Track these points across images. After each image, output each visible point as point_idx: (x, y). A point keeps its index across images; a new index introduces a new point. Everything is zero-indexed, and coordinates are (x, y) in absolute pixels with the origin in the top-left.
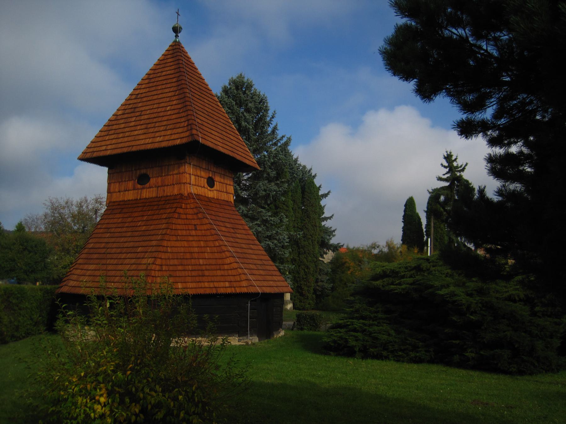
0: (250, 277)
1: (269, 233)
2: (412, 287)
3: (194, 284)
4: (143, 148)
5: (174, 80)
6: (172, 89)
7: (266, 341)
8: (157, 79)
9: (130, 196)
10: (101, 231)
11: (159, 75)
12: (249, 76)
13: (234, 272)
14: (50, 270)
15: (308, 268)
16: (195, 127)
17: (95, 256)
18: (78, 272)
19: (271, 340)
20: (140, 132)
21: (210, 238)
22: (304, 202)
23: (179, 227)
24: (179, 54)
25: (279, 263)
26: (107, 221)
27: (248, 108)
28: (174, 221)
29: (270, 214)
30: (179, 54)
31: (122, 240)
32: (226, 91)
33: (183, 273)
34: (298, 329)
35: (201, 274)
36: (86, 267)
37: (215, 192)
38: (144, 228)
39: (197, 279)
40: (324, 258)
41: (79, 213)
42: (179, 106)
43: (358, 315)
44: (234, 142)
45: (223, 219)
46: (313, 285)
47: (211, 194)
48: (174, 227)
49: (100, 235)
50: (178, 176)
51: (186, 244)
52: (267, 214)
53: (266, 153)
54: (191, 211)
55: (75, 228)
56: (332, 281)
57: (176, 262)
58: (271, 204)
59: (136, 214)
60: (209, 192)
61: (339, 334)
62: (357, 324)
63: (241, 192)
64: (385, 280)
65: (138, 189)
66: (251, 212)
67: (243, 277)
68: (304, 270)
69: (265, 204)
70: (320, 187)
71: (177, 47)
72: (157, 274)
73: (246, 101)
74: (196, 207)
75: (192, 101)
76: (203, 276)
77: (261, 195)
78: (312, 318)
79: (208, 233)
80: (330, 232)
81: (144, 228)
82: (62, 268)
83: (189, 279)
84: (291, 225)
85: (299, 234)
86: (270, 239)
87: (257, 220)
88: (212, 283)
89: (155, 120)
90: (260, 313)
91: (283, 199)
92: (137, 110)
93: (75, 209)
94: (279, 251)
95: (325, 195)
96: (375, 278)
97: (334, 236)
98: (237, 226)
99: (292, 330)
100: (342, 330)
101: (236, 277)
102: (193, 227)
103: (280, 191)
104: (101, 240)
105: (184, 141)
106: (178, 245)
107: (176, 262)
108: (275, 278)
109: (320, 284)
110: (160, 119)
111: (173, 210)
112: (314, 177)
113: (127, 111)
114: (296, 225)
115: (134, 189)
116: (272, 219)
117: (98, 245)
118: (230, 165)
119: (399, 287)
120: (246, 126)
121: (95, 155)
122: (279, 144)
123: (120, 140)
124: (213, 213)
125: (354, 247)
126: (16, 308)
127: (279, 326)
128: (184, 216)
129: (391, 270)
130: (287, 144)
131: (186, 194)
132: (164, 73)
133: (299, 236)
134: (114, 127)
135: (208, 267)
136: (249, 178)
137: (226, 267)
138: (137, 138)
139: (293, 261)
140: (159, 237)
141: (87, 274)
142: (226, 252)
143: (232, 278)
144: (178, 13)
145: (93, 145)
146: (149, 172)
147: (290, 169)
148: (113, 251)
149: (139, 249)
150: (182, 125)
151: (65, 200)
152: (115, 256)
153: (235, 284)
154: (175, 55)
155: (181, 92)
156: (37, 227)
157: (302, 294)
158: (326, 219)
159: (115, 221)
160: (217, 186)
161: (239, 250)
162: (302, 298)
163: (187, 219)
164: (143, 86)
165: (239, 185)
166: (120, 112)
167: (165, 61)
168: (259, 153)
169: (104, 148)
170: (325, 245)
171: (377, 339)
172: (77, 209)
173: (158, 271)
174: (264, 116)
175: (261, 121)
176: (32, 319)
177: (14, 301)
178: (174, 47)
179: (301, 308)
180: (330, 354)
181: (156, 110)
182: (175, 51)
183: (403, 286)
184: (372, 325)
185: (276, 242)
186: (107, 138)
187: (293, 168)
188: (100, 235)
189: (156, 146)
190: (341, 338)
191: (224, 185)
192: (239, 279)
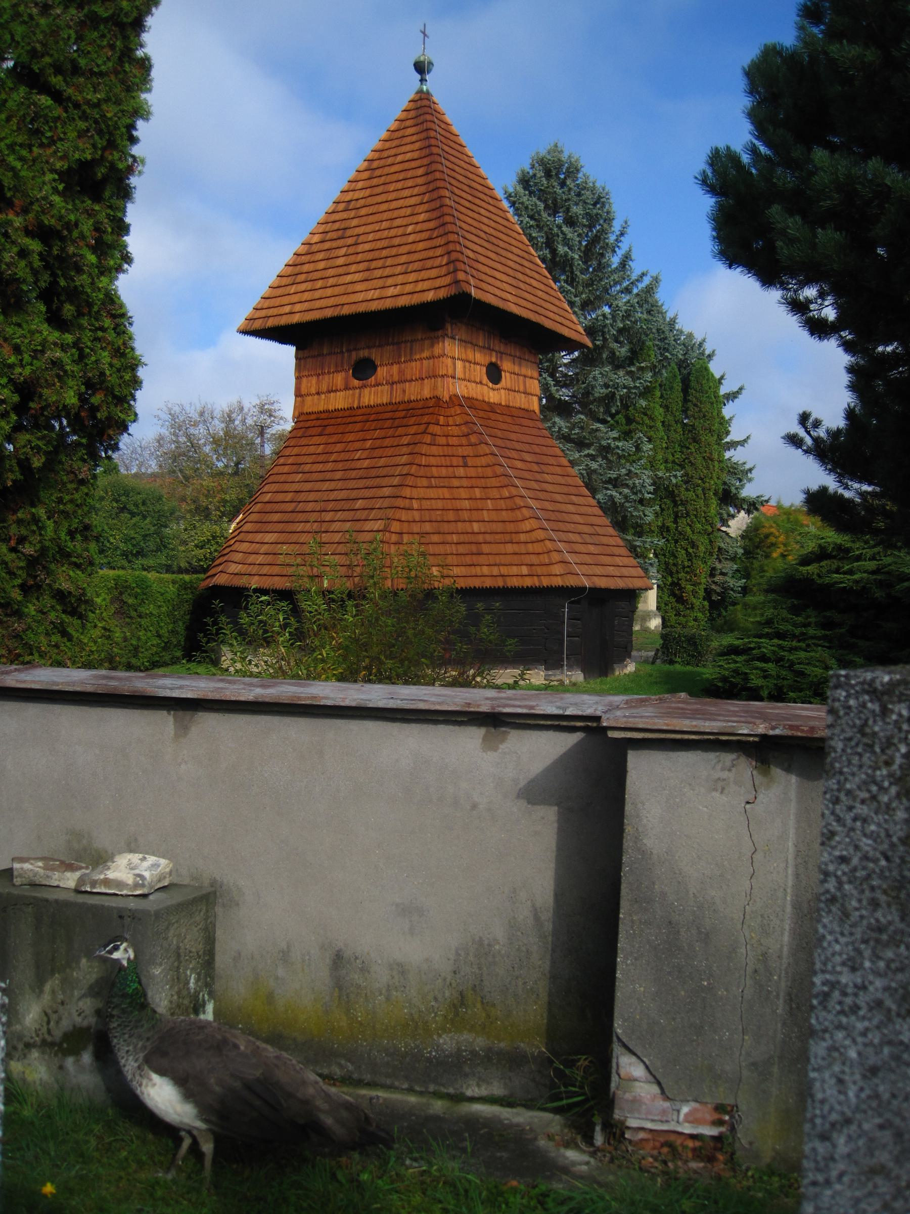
0: (569, 558)
1: (613, 474)
2: (875, 577)
3: (463, 568)
4: (362, 308)
5: (420, 171)
6: (416, 191)
7: (598, 680)
8: (387, 170)
9: (339, 401)
10: (286, 469)
11: (390, 161)
12: (571, 150)
13: (538, 548)
14: (173, 550)
15: (693, 545)
17: (276, 517)
18: (244, 547)
20: (357, 277)
21: (494, 482)
23: (433, 461)
24: (428, 117)
25: (634, 535)
26: (296, 451)
27: (571, 217)
28: (424, 449)
29: (615, 434)
30: (428, 117)
31: (326, 486)
32: (525, 181)
33: (441, 549)
34: (664, 662)
35: (475, 551)
36: (259, 537)
37: (503, 391)
38: (366, 463)
39: (468, 560)
40: (729, 526)
41: (227, 433)
42: (432, 225)
43: (770, 631)
44: (540, 294)
45: (518, 446)
46: (703, 581)
47: (494, 395)
48: (424, 461)
49: (282, 478)
50: (431, 361)
51: (446, 493)
52: (609, 436)
53: (606, 310)
54: (455, 430)
55: (220, 465)
57: (427, 527)
58: (618, 413)
59: (351, 437)
60: (491, 393)
61: (732, 666)
62: (768, 646)
63: (558, 391)
64: (823, 563)
65: (354, 388)
66: (577, 431)
67: (555, 557)
68: (686, 550)
69: (605, 413)
70: (722, 378)
71: (425, 103)
73: (566, 200)
74: (466, 423)
75: (456, 213)
77: (597, 395)
79: (489, 472)
80: (741, 473)
81: (366, 463)
82: (196, 546)
84: (660, 457)
85: (675, 476)
86: (615, 486)
87: (588, 446)
88: (496, 568)
89: (385, 253)
91: (643, 403)
92: (349, 233)
93: (218, 427)
94: (635, 512)
96: (805, 561)
97: (750, 480)
99: (653, 663)
101: (541, 556)
102: (460, 461)
103: (635, 387)
104: (287, 487)
105: (442, 294)
106: (432, 496)
108: (618, 561)
110: (394, 251)
111: (423, 427)
112: (710, 357)
113: (329, 236)
114: (671, 458)
115: (347, 388)
116: (620, 444)
117: (280, 497)
118: (532, 339)
119: (849, 577)
120: (566, 254)
121: (271, 323)
122: (635, 291)
123: (317, 294)
124: (499, 434)
125: (792, 505)
126: (134, 614)
127: (624, 652)
128: (443, 441)
129: (836, 544)
130: (650, 290)
131: (446, 398)
132: (400, 158)
133: (674, 481)
134: (306, 268)
135: (488, 538)
136: (573, 360)
137: (523, 537)
138: (350, 288)
139: (663, 530)
140: (396, 481)
141: (261, 551)
142: (524, 510)
143: (534, 559)
144: (424, 33)
145: (267, 303)
146: (375, 355)
147: (660, 340)
148: (310, 506)
149: (359, 504)
150: (438, 262)
151: (199, 409)
153: (539, 570)
154: (421, 119)
155: (435, 195)
156: (141, 465)
157: (680, 600)
158: (734, 445)
159: (312, 449)
161: (547, 505)
162: (681, 607)
163: (448, 445)
165: (552, 375)
166: (316, 238)
167: (400, 134)
168: (594, 310)
169: (287, 309)
170: (729, 498)
171: (801, 674)
172: (223, 425)
174: (603, 231)
175: (599, 243)
176: (159, 636)
177: (130, 601)
178: (419, 104)
181: (385, 234)
182: (420, 111)
183: (856, 577)
184: (796, 649)
185: (626, 491)
186: (293, 289)
187: (665, 338)
188: (282, 478)
189: (388, 304)
190: (736, 672)
191: (521, 378)
192: (547, 561)
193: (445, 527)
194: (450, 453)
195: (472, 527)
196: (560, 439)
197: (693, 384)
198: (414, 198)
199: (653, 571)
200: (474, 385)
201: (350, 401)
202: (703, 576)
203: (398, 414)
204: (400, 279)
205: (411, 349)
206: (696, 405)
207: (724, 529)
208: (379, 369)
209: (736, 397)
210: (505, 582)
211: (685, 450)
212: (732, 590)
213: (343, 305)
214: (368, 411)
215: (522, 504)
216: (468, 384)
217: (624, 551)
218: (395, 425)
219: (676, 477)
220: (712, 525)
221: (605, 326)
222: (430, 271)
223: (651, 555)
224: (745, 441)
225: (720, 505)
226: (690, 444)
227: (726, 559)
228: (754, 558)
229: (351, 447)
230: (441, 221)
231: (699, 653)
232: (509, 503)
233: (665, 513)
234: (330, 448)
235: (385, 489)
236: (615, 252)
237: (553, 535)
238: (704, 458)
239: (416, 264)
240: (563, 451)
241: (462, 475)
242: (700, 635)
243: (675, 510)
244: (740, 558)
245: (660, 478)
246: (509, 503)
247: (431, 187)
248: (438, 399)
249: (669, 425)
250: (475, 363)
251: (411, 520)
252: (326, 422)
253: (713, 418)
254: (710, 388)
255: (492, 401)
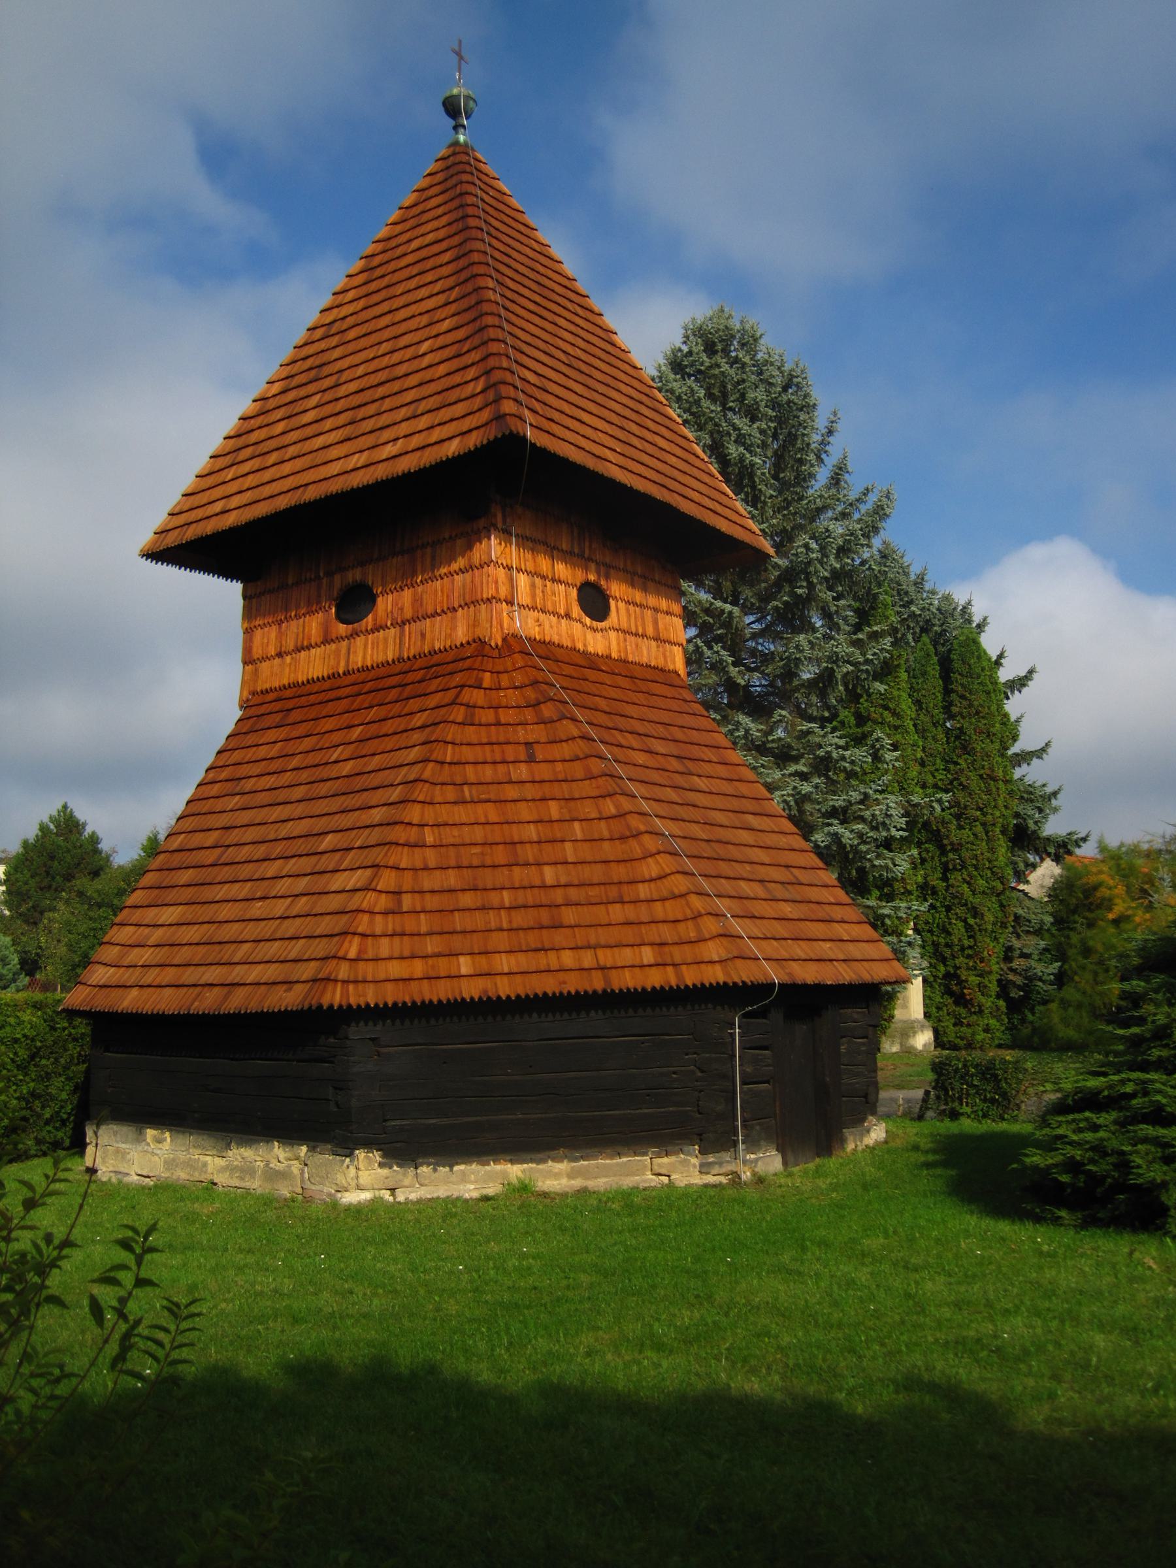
0: (737, 927)
1: (838, 801)
3: (521, 957)
4: (335, 487)
8: (393, 266)
9: (314, 665)
11: (399, 251)
13: (671, 910)
15: (975, 912)
16: (512, 392)
17: (186, 876)
19: (832, 1163)
21: (587, 788)
22: (951, 704)
23: (468, 753)
24: (465, 177)
25: (880, 899)
28: (451, 733)
30: (465, 177)
32: (677, 364)
33: (478, 920)
36: (150, 915)
37: (613, 635)
38: (347, 768)
39: (532, 939)
40: (1028, 882)
42: (461, 334)
43: (1165, 1053)
44: (673, 460)
46: (995, 968)
48: (449, 754)
50: (468, 576)
51: (492, 813)
54: (513, 697)
56: (1059, 953)
57: (452, 879)
59: (330, 724)
60: (590, 635)
61: (1089, 1136)
67: (710, 926)
68: (965, 921)
70: (1001, 656)
72: (379, 924)
74: (535, 683)
75: (502, 312)
76: (557, 926)
78: (989, 1072)
79: (578, 769)
80: (1041, 800)
83: (500, 940)
85: (940, 801)
86: (843, 822)
87: (796, 759)
89: (381, 391)
90: (790, 1054)
91: (882, 688)
95: (1020, 683)
97: (1055, 810)
98: (696, 752)
100: (1104, 1118)
101: (681, 927)
102: (522, 754)
103: (867, 661)
105: (473, 441)
106: (464, 819)
107: (452, 879)
108: (841, 930)
109: (1018, 963)
110: (396, 386)
111: (451, 695)
112: (981, 627)
115: (326, 641)
120: (742, 459)
124: (603, 704)
125: (1122, 845)
127: (865, 1104)
132: (415, 245)
134: (254, 437)
135: (573, 893)
137: (643, 891)
139: (926, 890)
140: (395, 794)
142: (646, 838)
143: (666, 933)
146: (370, 575)
148: (244, 853)
149: (328, 842)
150: (469, 389)
152: (246, 871)
153: (677, 954)
155: (469, 287)
157: (961, 1000)
158: (1025, 757)
159: (262, 752)
160: (618, 613)
163: (498, 724)
164: (350, 295)
166: (276, 388)
169: (218, 507)
170: (1025, 838)
173: (386, 913)
179: (962, 1043)
180: (1056, 1221)
181: (386, 361)
182: (451, 171)
189: (381, 472)
190: (1099, 1149)
192: (693, 935)
193: (488, 878)
194: (502, 739)
195: (542, 874)
196: (750, 750)
197: (957, 665)
198: (434, 299)
199: (914, 955)
200: (554, 619)
201: (332, 662)
202: (994, 960)
203: (411, 677)
204: (404, 428)
205: (433, 558)
206: (963, 697)
207: (1021, 887)
208: (380, 600)
209: (1024, 685)
210: (607, 980)
211: (952, 767)
212: (1040, 979)
213: (306, 485)
214: (362, 676)
215: (642, 828)
216: (542, 616)
217: (867, 931)
218: (405, 695)
219: (938, 805)
220: (1002, 879)
221: (809, 563)
222: (454, 407)
223: (910, 932)
224: (1043, 750)
225: (1011, 849)
226: (959, 756)
227: (1028, 932)
228: (1071, 929)
229: (326, 741)
230: (477, 325)
231: (1004, 1095)
232: (618, 827)
233: (928, 865)
234: (291, 747)
235: (374, 811)
236: (822, 461)
237: (706, 885)
238: (981, 776)
239: (432, 400)
240: (755, 768)
241: (524, 777)
242: (1004, 1062)
243: (944, 859)
244: (1048, 930)
245: (915, 805)
246: (618, 827)
247: (463, 276)
248: (481, 642)
249: (924, 730)
250: (553, 580)
251: (419, 865)
252: (290, 704)
253: (991, 714)
254: (983, 669)
255: (590, 649)
